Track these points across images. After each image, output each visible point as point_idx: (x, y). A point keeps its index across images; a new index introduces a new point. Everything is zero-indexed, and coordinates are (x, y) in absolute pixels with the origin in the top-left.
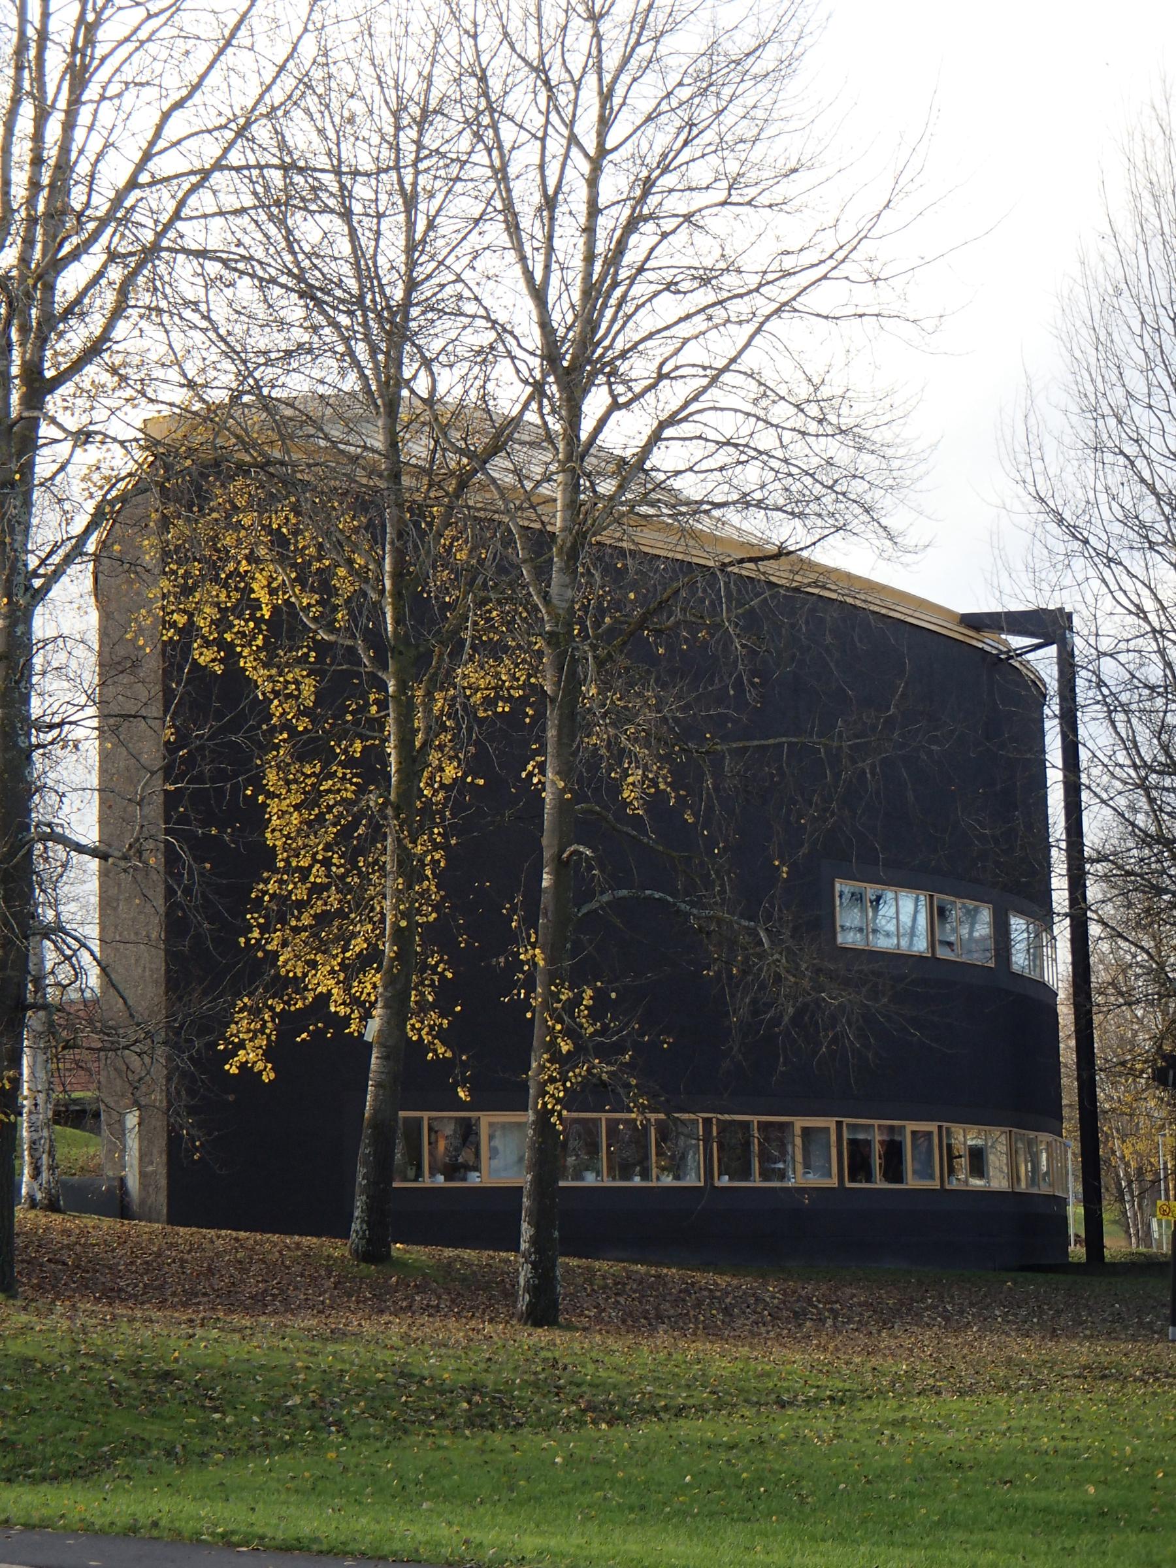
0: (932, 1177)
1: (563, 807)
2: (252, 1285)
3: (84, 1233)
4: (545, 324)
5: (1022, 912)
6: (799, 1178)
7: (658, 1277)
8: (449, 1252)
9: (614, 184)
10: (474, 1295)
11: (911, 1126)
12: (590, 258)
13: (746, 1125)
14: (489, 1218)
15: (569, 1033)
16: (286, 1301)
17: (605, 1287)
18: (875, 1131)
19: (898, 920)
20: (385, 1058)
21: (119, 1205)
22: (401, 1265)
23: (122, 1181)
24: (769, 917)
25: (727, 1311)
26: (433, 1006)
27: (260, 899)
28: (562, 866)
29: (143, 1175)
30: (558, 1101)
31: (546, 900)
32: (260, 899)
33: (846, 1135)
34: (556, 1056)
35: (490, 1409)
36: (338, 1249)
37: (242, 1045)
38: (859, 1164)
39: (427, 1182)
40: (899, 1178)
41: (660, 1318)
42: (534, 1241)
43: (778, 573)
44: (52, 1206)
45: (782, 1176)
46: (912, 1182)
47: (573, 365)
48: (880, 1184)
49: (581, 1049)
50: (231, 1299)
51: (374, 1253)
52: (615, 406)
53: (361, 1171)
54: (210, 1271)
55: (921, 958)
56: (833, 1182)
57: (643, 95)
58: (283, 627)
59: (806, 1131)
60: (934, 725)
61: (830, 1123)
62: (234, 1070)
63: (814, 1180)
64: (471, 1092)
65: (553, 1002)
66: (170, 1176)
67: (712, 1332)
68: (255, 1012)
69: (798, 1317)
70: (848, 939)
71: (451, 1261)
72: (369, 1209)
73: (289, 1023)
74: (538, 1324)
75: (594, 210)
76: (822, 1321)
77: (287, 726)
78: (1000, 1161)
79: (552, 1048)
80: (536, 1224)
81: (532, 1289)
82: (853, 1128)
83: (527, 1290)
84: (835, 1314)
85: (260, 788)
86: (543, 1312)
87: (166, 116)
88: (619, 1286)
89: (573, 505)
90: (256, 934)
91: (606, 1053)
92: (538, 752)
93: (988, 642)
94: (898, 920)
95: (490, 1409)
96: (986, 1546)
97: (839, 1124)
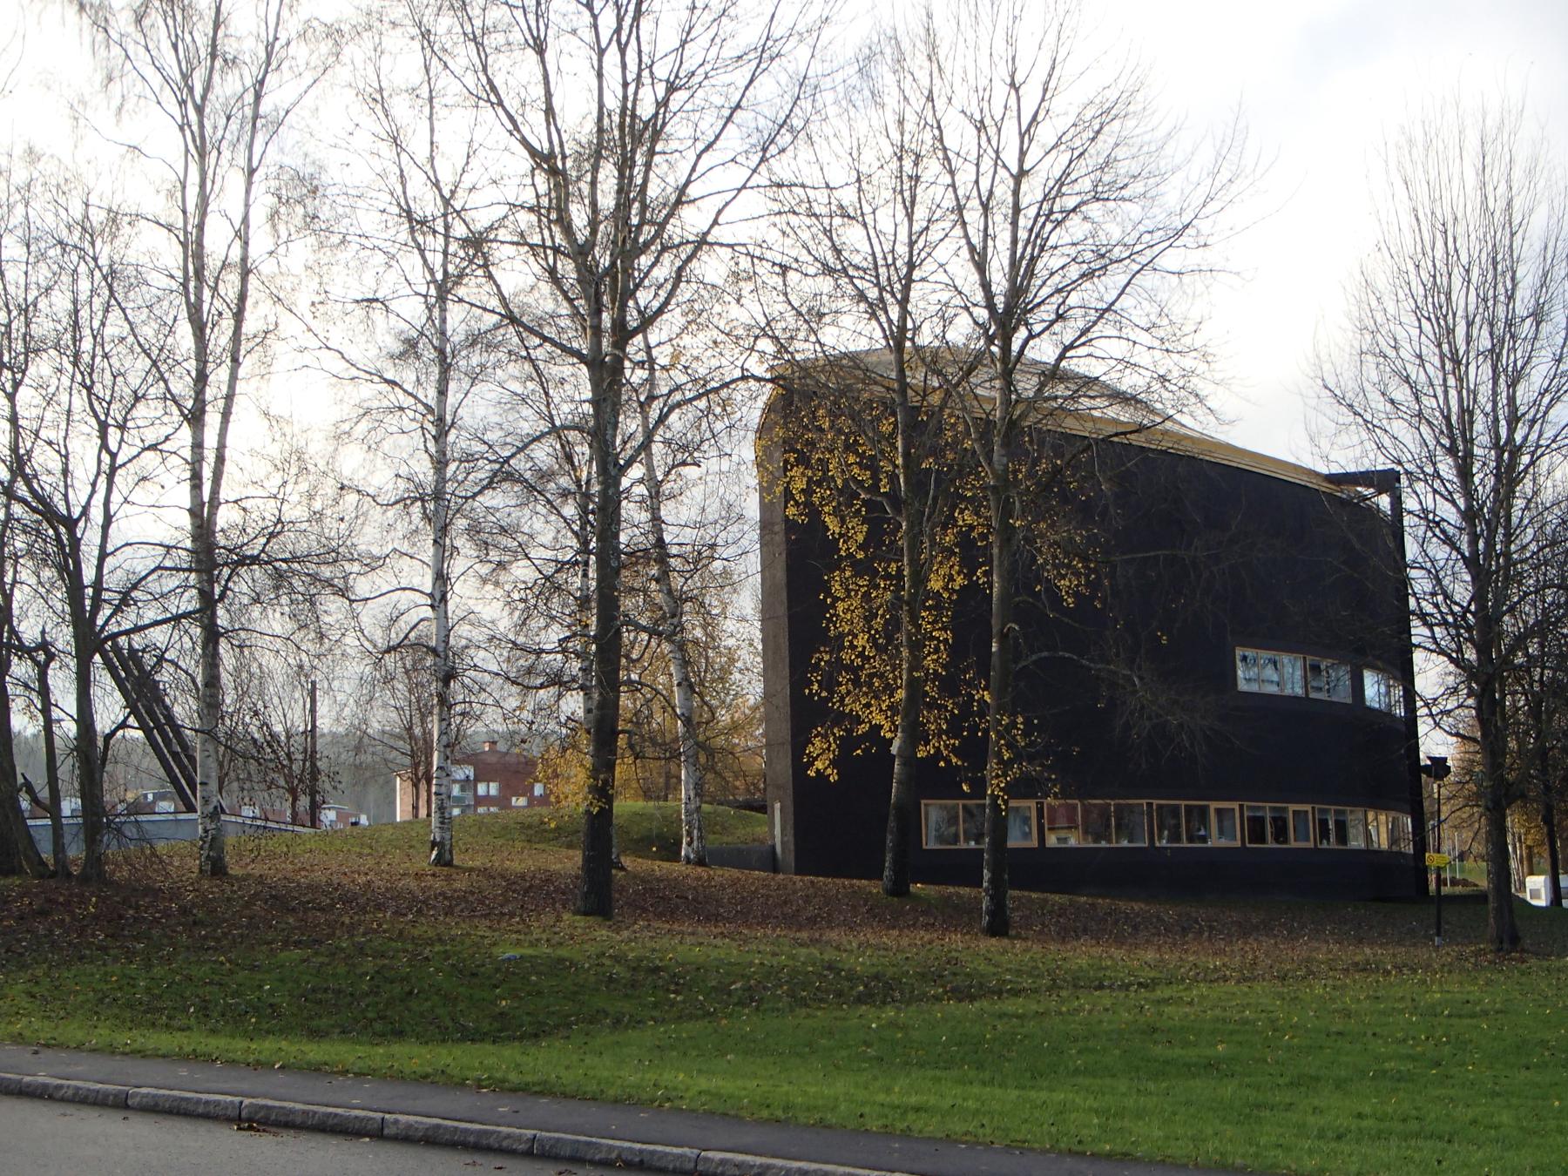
0: (1308, 840)
1: (1005, 597)
2: (811, 911)
3: (710, 879)
4: (986, 286)
5: (1373, 667)
6: (1215, 841)
7: (1092, 905)
8: (951, 889)
9: (1032, 192)
10: (955, 916)
11: (1292, 807)
12: (1015, 241)
13: (1178, 807)
14: (960, 868)
15: (1009, 746)
16: (829, 922)
17: (1050, 912)
18: (1267, 809)
19: (1268, 674)
20: (903, 764)
21: (771, 862)
22: (916, 897)
23: (774, 847)
24: (1140, 669)
25: (1135, 928)
26: (946, 732)
27: (818, 664)
28: (1003, 637)
29: (783, 843)
30: (1001, 789)
31: (995, 660)
32: (818, 664)
33: (1246, 814)
34: (1001, 761)
35: (880, 989)
36: (874, 887)
37: (815, 759)
38: (1256, 829)
39: (962, 845)
40: (1286, 841)
41: (1085, 931)
42: (991, 881)
43: (1137, 440)
44: (700, 862)
45: (1204, 839)
46: (1293, 844)
47: (1009, 315)
48: (1271, 844)
49: (1018, 756)
50: (792, 921)
51: (899, 889)
52: (1031, 337)
53: (889, 837)
54: (785, 902)
55: (1294, 699)
56: (1238, 844)
57: (1046, 134)
58: (848, 494)
59: (1218, 811)
60: (1302, 548)
61: (1235, 805)
62: (813, 774)
63: (1224, 843)
64: (970, 787)
65: (1005, 730)
66: (796, 844)
67: (1120, 941)
68: (825, 736)
69: (1184, 931)
70: (1243, 686)
71: (950, 896)
72: (895, 862)
73: (847, 744)
74: (993, 935)
75: (1017, 210)
76: (1201, 933)
77: (850, 556)
78: (1378, 830)
79: (999, 755)
80: (992, 871)
81: (991, 913)
82: (1249, 808)
83: (988, 913)
84: (1211, 928)
85: (828, 593)
86: (999, 927)
87: (699, 157)
88: (1062, 912)
89: (1007, 402)
90: (816, 687)
91: (1031, 759)
92: (983, 564)
93: (1343, 493)
94: (1268, 674)
95: (880, 989)
96: (755, 1075)
97: (1241, 807)
